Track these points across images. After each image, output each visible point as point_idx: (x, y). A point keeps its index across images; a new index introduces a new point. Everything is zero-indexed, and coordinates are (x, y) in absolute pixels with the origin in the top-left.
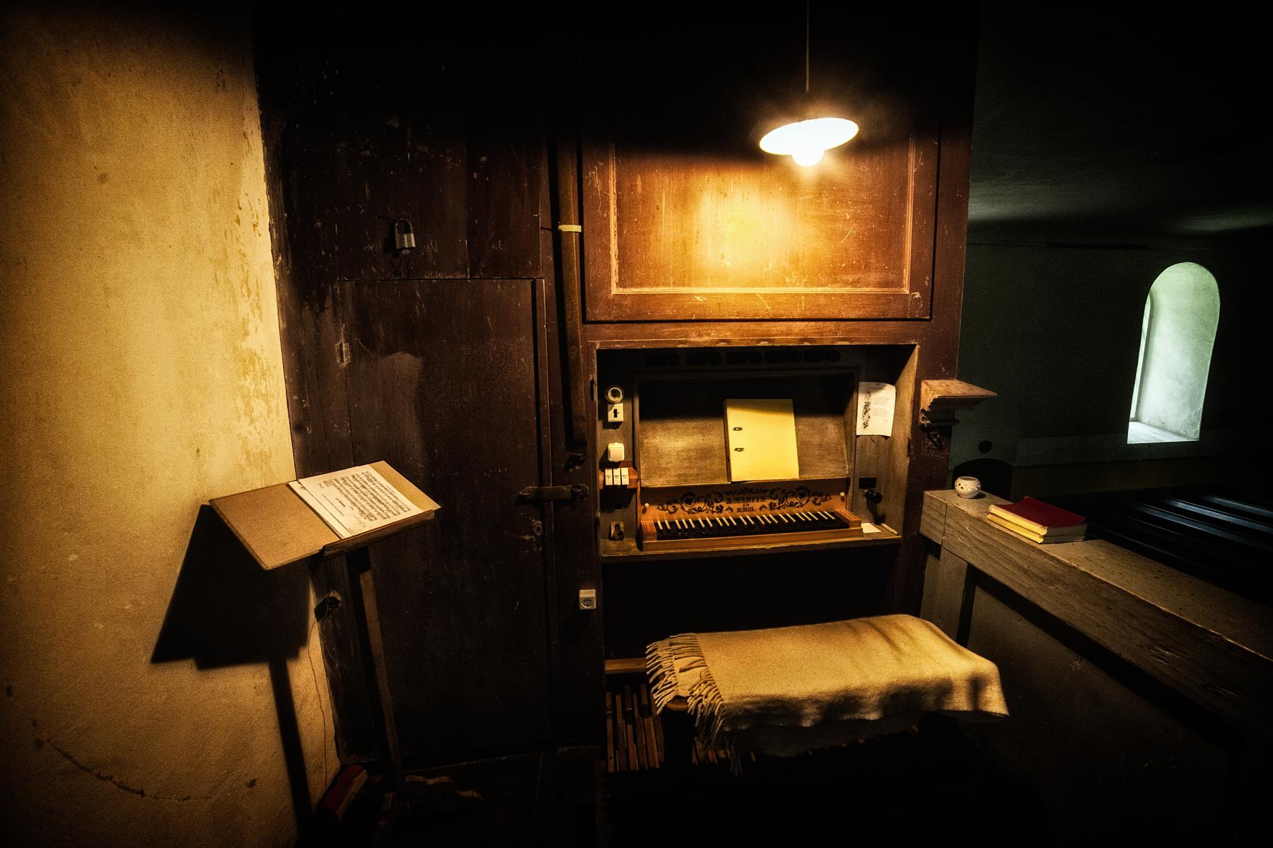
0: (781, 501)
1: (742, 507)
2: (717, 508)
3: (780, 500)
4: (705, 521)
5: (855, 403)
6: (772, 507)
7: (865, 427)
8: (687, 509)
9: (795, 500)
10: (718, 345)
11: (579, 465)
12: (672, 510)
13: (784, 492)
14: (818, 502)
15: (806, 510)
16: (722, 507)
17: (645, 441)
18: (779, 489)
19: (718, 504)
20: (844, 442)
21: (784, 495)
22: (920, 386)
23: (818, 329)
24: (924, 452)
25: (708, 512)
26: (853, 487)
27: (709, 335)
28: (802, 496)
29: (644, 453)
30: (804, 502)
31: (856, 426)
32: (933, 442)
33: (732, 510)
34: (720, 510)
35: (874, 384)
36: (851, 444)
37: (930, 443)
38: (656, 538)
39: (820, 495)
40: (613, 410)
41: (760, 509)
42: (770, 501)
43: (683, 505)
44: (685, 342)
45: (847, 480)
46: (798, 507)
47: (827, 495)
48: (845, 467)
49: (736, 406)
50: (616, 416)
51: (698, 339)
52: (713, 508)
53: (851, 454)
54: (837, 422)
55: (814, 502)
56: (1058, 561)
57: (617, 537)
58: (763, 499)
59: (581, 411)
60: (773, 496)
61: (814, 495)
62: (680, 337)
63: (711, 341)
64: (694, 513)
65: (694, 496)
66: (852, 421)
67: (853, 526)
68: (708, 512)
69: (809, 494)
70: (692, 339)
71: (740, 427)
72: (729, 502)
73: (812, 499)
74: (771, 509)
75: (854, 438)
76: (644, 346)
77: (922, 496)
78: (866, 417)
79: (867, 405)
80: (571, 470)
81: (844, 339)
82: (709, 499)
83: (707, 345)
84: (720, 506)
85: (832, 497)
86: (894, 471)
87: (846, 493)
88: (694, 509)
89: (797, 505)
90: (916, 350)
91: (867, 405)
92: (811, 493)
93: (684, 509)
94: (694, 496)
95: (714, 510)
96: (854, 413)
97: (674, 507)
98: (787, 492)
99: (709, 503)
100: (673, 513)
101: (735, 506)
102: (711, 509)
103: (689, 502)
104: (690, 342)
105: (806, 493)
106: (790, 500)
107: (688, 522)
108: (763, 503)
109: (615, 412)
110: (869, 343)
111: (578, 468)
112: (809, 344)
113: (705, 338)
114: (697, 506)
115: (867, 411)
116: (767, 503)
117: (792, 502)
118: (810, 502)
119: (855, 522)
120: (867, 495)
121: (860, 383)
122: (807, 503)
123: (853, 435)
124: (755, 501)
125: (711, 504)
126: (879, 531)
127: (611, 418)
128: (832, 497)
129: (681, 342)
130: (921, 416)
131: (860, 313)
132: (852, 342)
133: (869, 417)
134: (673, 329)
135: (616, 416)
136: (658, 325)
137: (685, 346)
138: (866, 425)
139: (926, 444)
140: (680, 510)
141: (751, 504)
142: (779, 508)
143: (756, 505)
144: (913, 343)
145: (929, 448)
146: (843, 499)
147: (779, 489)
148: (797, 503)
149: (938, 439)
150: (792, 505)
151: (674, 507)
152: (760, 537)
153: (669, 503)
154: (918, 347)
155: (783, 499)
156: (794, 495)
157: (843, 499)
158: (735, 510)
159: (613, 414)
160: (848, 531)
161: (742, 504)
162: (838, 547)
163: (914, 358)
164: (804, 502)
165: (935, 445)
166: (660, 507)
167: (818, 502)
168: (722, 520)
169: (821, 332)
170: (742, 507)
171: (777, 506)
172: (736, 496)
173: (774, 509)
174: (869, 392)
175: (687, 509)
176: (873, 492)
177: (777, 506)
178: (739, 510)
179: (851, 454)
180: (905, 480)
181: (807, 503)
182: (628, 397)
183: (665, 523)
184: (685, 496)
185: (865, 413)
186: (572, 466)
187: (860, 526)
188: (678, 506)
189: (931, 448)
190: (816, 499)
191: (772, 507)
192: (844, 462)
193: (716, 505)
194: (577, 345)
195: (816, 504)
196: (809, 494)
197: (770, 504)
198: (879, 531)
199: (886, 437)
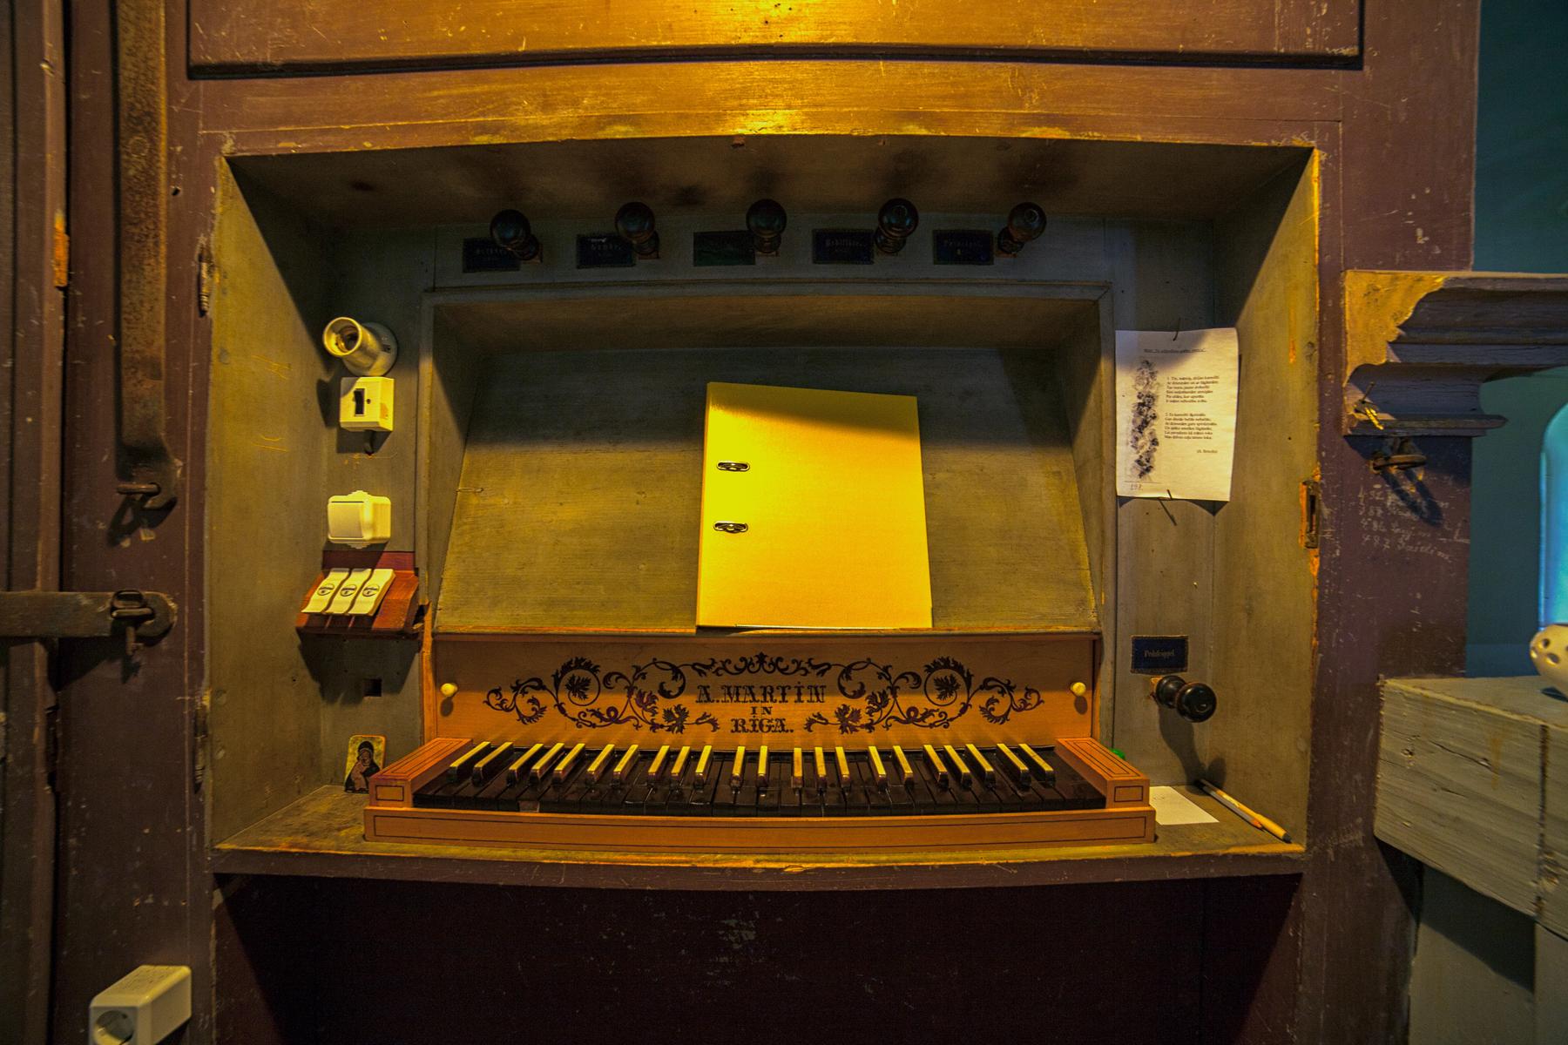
0: (878, 702)
1: (747, 716)
2: (668, 714)
3: (872, 698)
4: (888, 756)
5: (1106, 394)
6: (847, 720)
7: (1142, 474)
8: (573, 710)
9: (921, 702)
10: (601, 135)
11: (151, 526)
12: (527, 710)
13: (884, 673)
14: (999, 710)
15: (963, 736)
16: (683, 713)
17: (474, 501)
18: (869, 662)
19: (671, 704)
20: (1080, 526)
21: (885, 684)
22: (1338, 293)
23: (953, 84)
24: (1370, 532)
25: (637, 727)
26: (1115, 663)
27: (575, 103)
28: (947, 688)
29: (461, 534)
30: (953, 710)
31: (1114, 467)
32: (1403, 495)
33: (714, 723)
34: (677, 720)
35: (1161, 338)
36: (1102, 522)
37: (1392, 498)
38: (409, 797)
39: (1008, 688)
40: (351, 395)
41: (809, 725)
42: (840, 701)
43: (563, 697)
44: (495, 129)
45: (1094, 643)
46: (932, 725)
47: (1029, 691)
48: (1083, 602)
49: (733, 404)
50: (359, 410)
51: (538, 118)
52: (655, 713)
53: (1102, 556)
54: (1055, 469)
55: (987, 712)
56: (1387, 834)
57: (360, 782)
58: (817, 692)
59: (150, 344)
60: (851, 687)
61: (985, 686)
62: (483, 114)
63: (583, 123)
64: (593, 726)
65: (595, 670)
66: (1099, 455)
67: (1116, 802)
68: (637, 727)
69: (969, 685)
70: (520, 119)
71: (744, 462)
72: (706, 695)
73: (980, 700)
74: (843, 729)
75: (1109, 505)
76: (368, 145)
77: (1374, 699)
78: (1144, 441)
79: (1145, 406)
80: (126, 543)
81: (1051, 120)
82: (639, 684)
83: (565, 135)
84: (678, 708)
85: (1044, 696)
86: (1250, 613)
87: (1092, 686)
88: (596, 713)
89: (929, 720)
90: (1314, 169)
91: (1145, 406)
92: (976, 682)
93: (563, 711)
94: (595, 670)
95: (659, 719)
96: (1106, 424)
97: (533, 701)
98: (894, 674)
99: (641, 695)
100: (530, 719)
101: (728, 711)
102: (648, 716)
103: (578, 688)
104: (514, 129)
105: (960, 680)
106: (905, 701)
107: (830, 757)
108: (817, 708)
109: (359, 396)
110: (1139, 138)
111: (146, 535)
112: (923, 132)
113: (566, 114)
114: (605, 701)
115: (1145, 423)
116: (831, 705)
117: (913, 709)
118: (974, 712)
119: (1126, 785)
120: (1162, 696)
121: (1118, 333)
122: (963, 711)
123: (1106, 494)
124: (791, 698)
125: (646, 701)
126: (1213, 820)
127: (347, 414)
128: (1044, 696)
129: (483, 129)
130: (1353, 397)
131: (1101, 30)
132: (1078, 130)
133: (1155, 442)
134: (466, 90)
135: (359, 410)
136: (415, 79)
137: (498, 140)
138: (1145, 467)
139: (1376, 503)
140: (552, 711)
141: (778, 710)
142: (870, 727)
143: (794, 711)
144: (1299, 141)
145: (1388, 519)
146: (1080, 704)
147: (869, 662)
148: (928, 713)
149: (1420, 486)
150: (912, 717)
151: (533, 701)
152: (762, 827)
153: (518, 688)
154: (1317, 157)
155: (883, 695)
156: (918, 684)
157: (1080, 704)
158: (725, 723)
159: (353, 405)
160: (1099, 819)
161: (748, 707)
162: (1064, 879)
163: (1312, 166)
164: (953, 710)
165: (1414, 507)
166: (494, 699)
167: (999, 710)
168: (943, 755)
169: (964, 96)
170: (747, 716)
171: (865, 719)
172: (726, 679)
173: (854, 729)
174: (1148, 364)
175: (573, 710)
176: (1181, 683)
177: (865, 719)
178: (738, 726)
179: (1102, 556)
180: (1303, 637)
181: (963, 711)
182: (401, 364)
183: (813, 754)
184: (567, 668)
185: (1141, 429)
186: (131, 530)
187: (1143, 798)
188: (545, 698)
189: (1397, 517)
190: (991, 701)
191: (847, 720)
192: (1079, 585)
193: (662, 704)
194: (151, 133)
195: (996, 719)
196: (969, 685)
197: (841, 712)
198: (1213, 820)
199: (1213, 507)
